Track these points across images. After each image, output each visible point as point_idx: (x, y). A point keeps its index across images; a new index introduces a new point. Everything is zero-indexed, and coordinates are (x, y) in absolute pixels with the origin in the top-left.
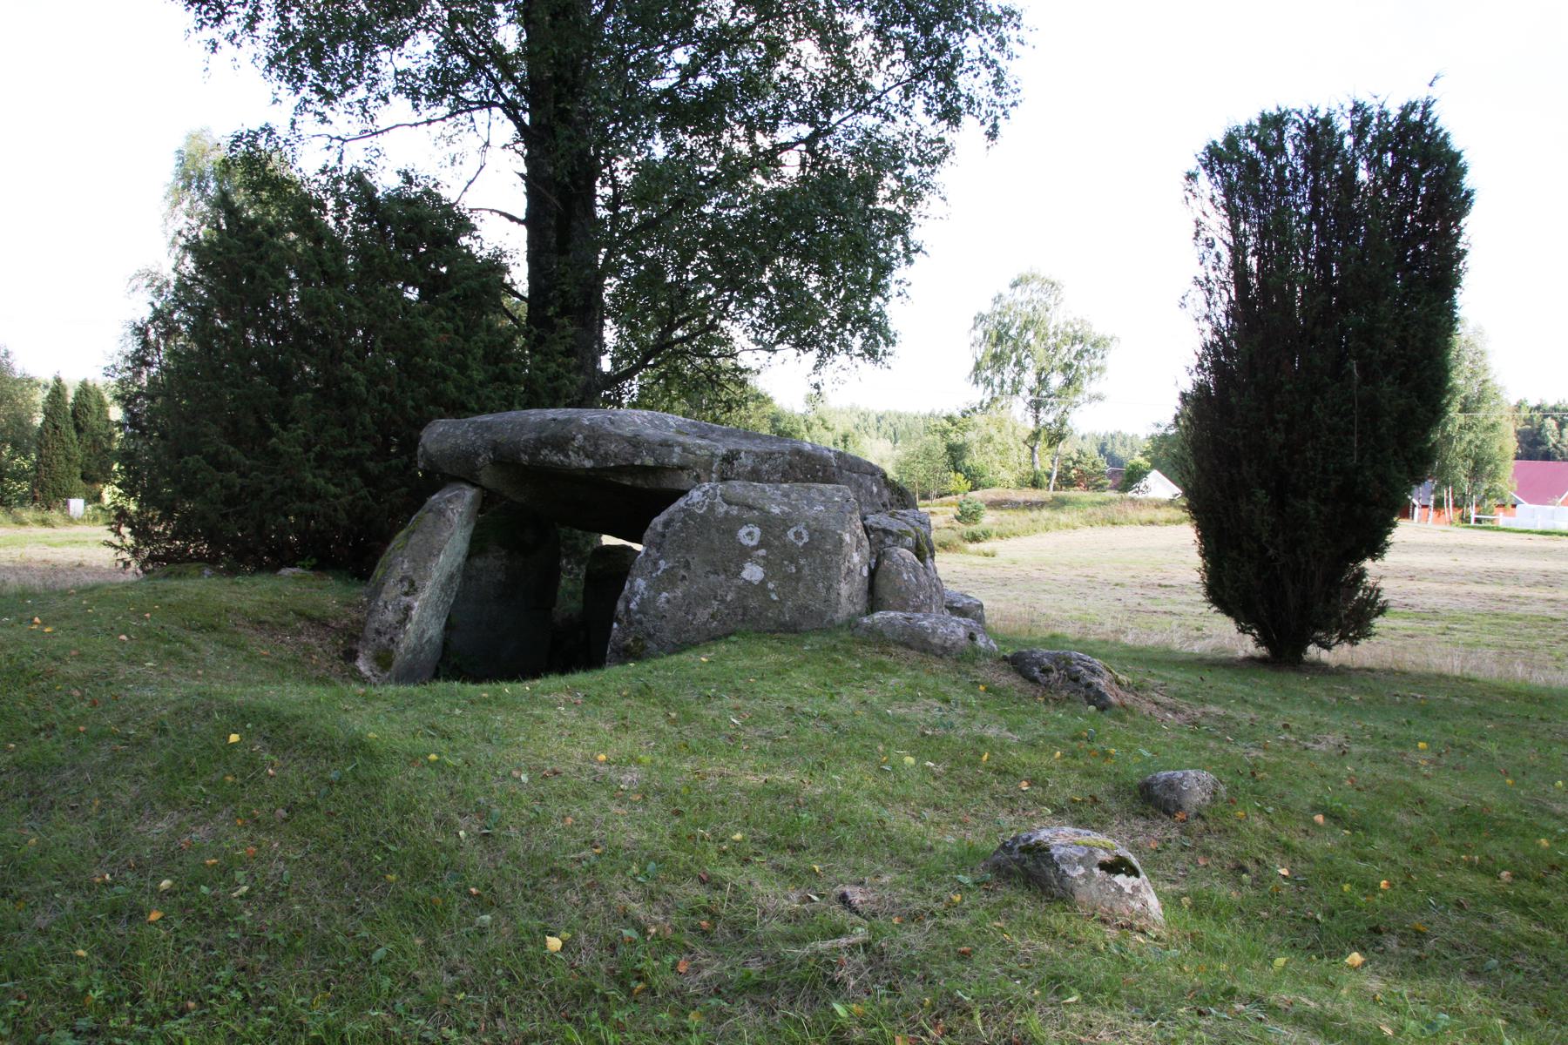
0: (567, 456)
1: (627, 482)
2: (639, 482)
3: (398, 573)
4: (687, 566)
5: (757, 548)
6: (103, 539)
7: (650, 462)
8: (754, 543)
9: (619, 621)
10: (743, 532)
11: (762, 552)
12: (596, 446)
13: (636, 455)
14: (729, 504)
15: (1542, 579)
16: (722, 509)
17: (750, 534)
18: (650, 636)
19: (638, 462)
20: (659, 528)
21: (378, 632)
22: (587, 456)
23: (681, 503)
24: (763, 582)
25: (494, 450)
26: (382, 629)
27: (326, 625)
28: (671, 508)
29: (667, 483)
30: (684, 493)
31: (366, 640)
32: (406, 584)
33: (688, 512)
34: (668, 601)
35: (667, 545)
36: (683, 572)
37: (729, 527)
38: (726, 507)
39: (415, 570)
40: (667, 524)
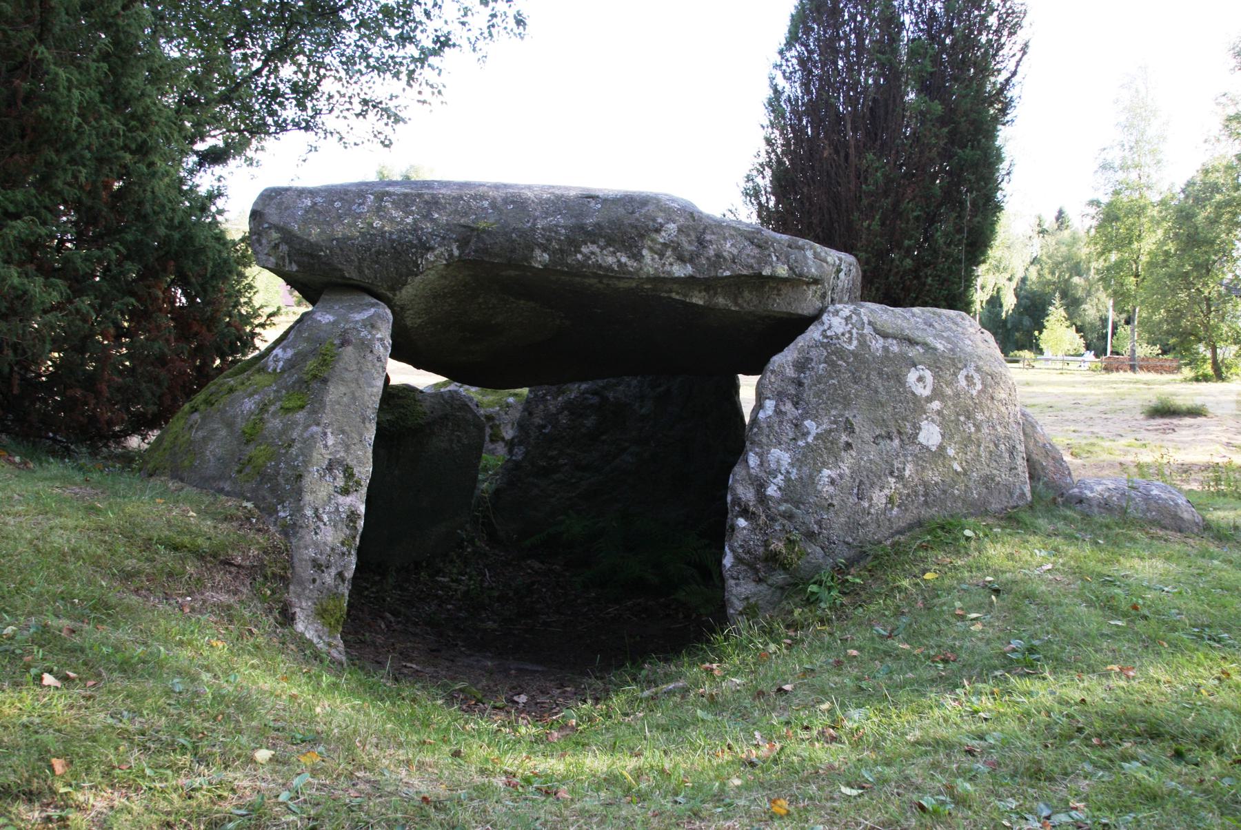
0: (638, 257)
1: (698, 299)
2: (721, 301)
3: (321, 456)
4: (849, 428)
5: (929, 399)
6: (1044, 217)
7: (782, 271)
8: (927, 392)
9: (745, 513)
10: (912, 376)
11: (936, 405)
12: (701, 243)
13: (763, 260)
14: (885, 336)
15: (1180, 445)
16: (877, 344)
17: (920, 379)
18: (810, 536)
19: (767, 271)
20: (790, 372)
21: (317, 566)
22: (681, 259)
23: (814, 333)
24: (941, 448)
25: (463, 243)
26: (322, 559)
27: (227, 563)
28: (801, 341)
29: (780, 304)
30: (815, 318)
31: (301, 583)
32: (340, 475)
33: (829, 343)
34: (832, 482)
35: (809, 395)
36: (844, 438)
37: (893, 369)
38: (881, 340)
39: (347, 448)
40: (802, 365)
